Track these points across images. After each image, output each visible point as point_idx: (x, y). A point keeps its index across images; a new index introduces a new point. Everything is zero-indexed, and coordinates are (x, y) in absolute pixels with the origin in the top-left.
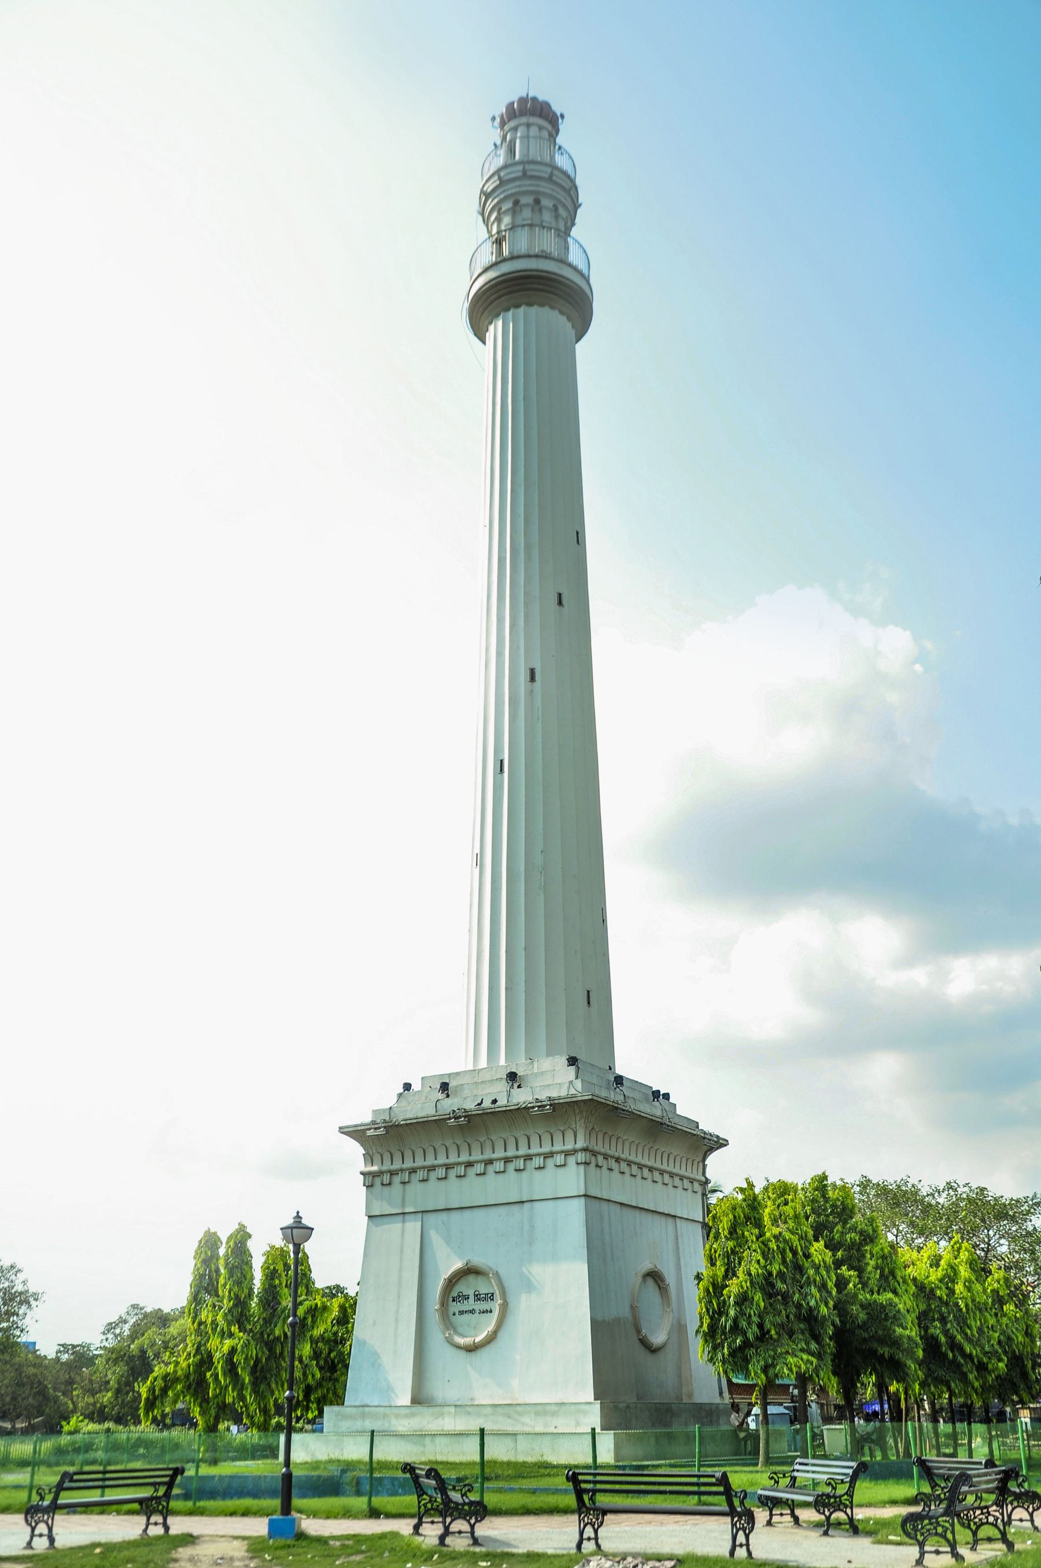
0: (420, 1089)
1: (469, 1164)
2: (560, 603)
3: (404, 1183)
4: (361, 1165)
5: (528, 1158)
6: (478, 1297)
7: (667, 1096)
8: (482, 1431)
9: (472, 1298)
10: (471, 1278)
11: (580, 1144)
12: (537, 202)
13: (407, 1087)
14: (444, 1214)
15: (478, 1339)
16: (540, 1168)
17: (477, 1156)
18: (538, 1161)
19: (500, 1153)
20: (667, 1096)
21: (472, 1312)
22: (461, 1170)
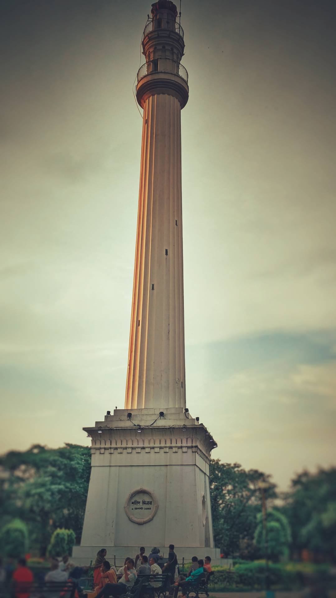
6: (144, 503)
8: (183, 558)
10: (141, 495)
12: (164, 47)
14: (130, 468)
15: (145, 520)
17: (146, 445)
19: (157, 445)
21: (142, 508)
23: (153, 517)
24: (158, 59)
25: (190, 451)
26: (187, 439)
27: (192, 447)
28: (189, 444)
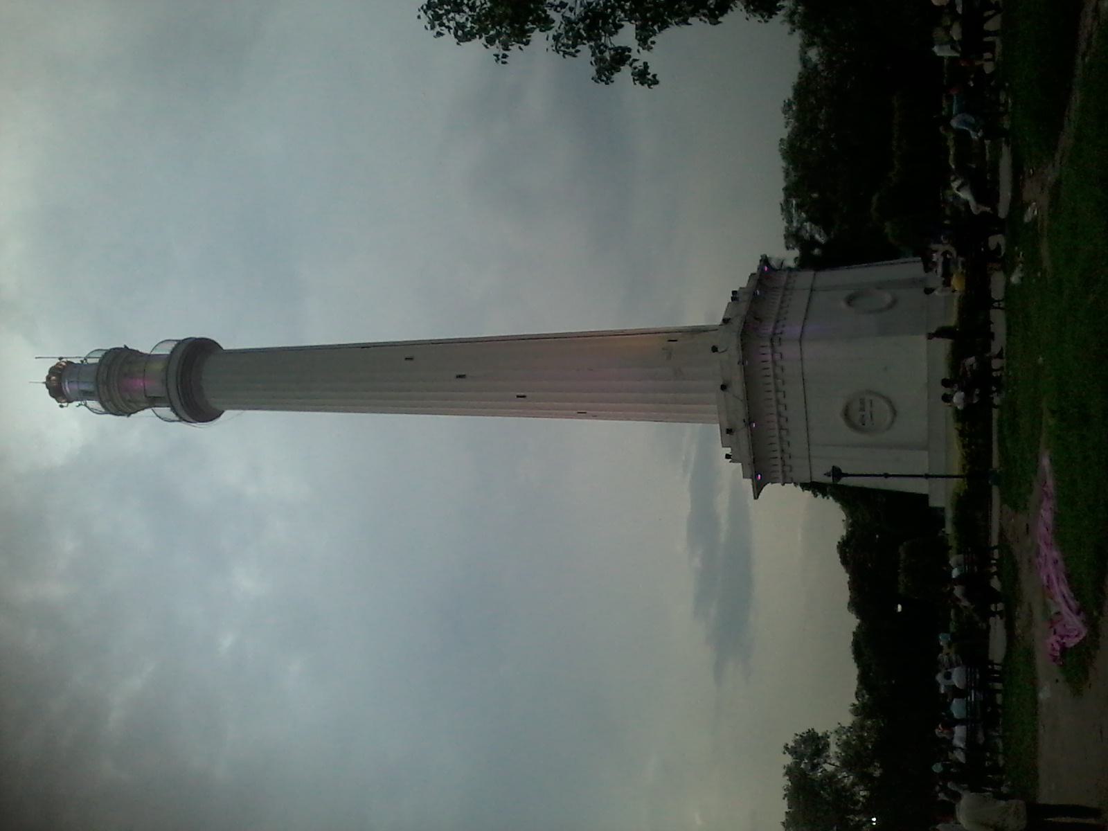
0: (730, 449)
1: (779, 415)
2: (411, 359)
3: (790, 457)
4: (778, 485)
5: (776, 376)
6: (863, 409)
7: (734, 293)
9: (864, 413)
11: (768, 344)
13: (728, 456)
16: (782, 369)
17: (774, 410)
18: (778, 371)
19: (772, 395)
20: (734, 293)
22: (783, 420)
23: (884, 397)
24: (146, 396)
25: (779, 349)
26: (768, 422)
27: (772, 346)
28: (769, 351)
